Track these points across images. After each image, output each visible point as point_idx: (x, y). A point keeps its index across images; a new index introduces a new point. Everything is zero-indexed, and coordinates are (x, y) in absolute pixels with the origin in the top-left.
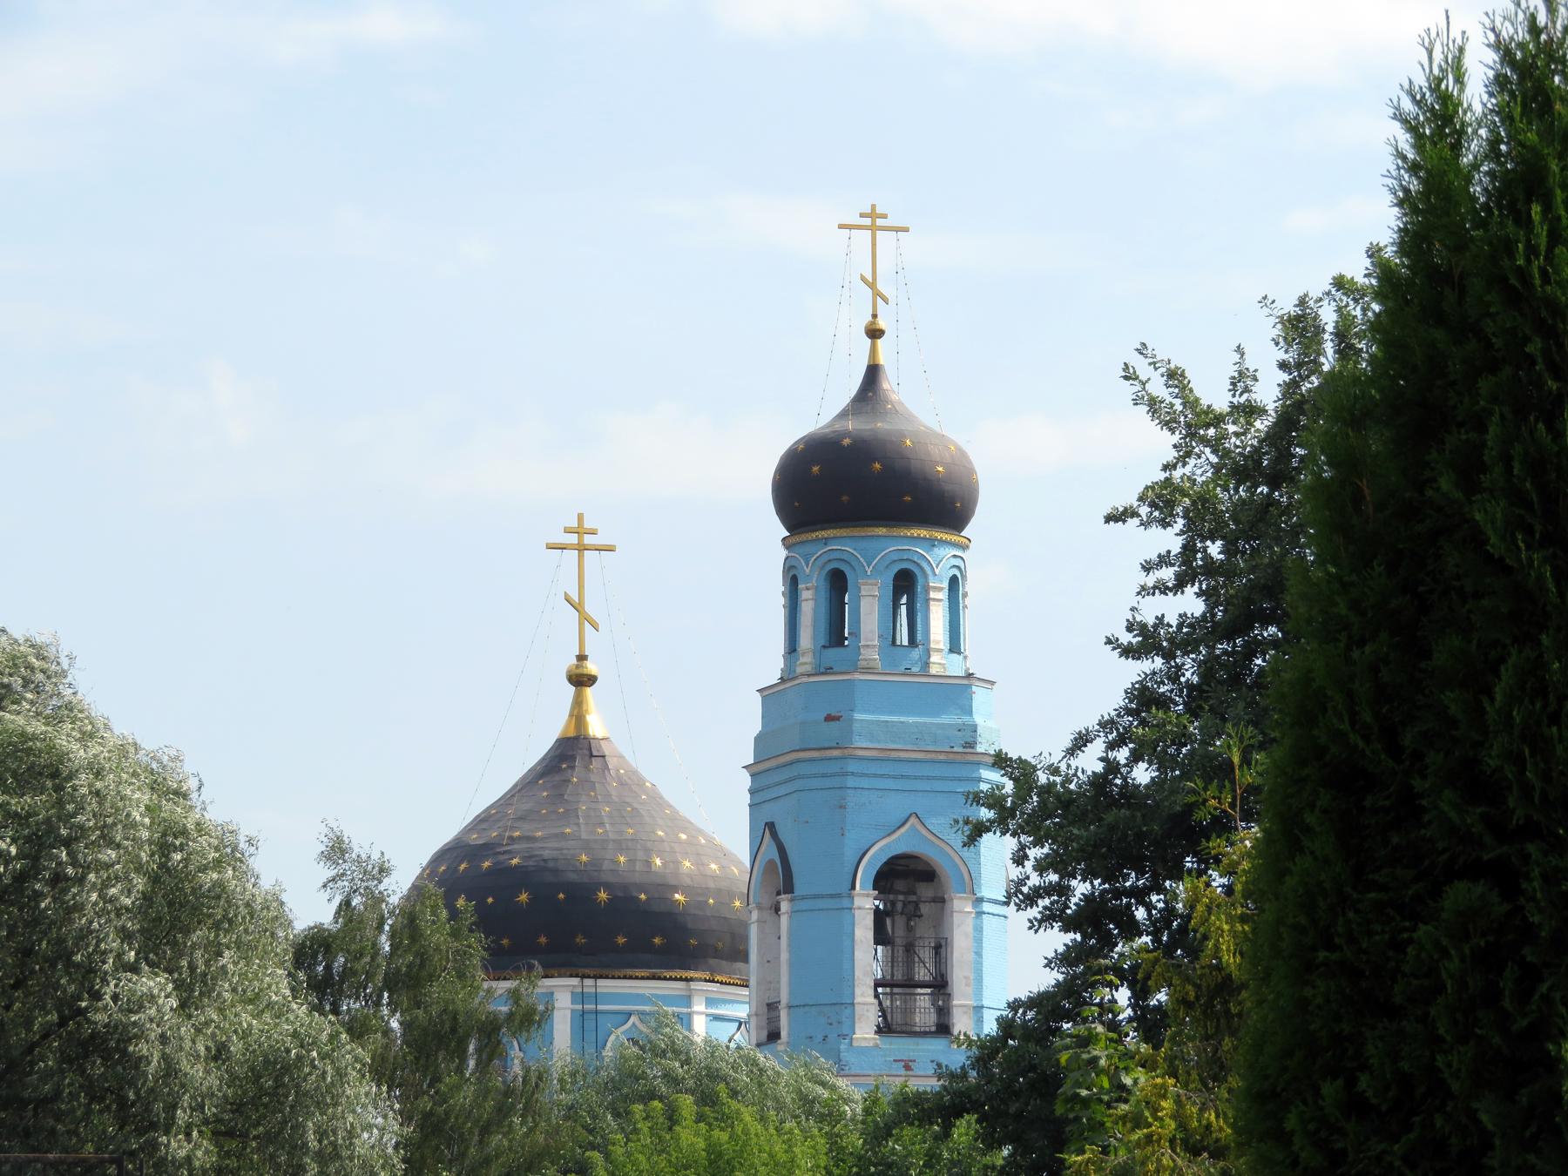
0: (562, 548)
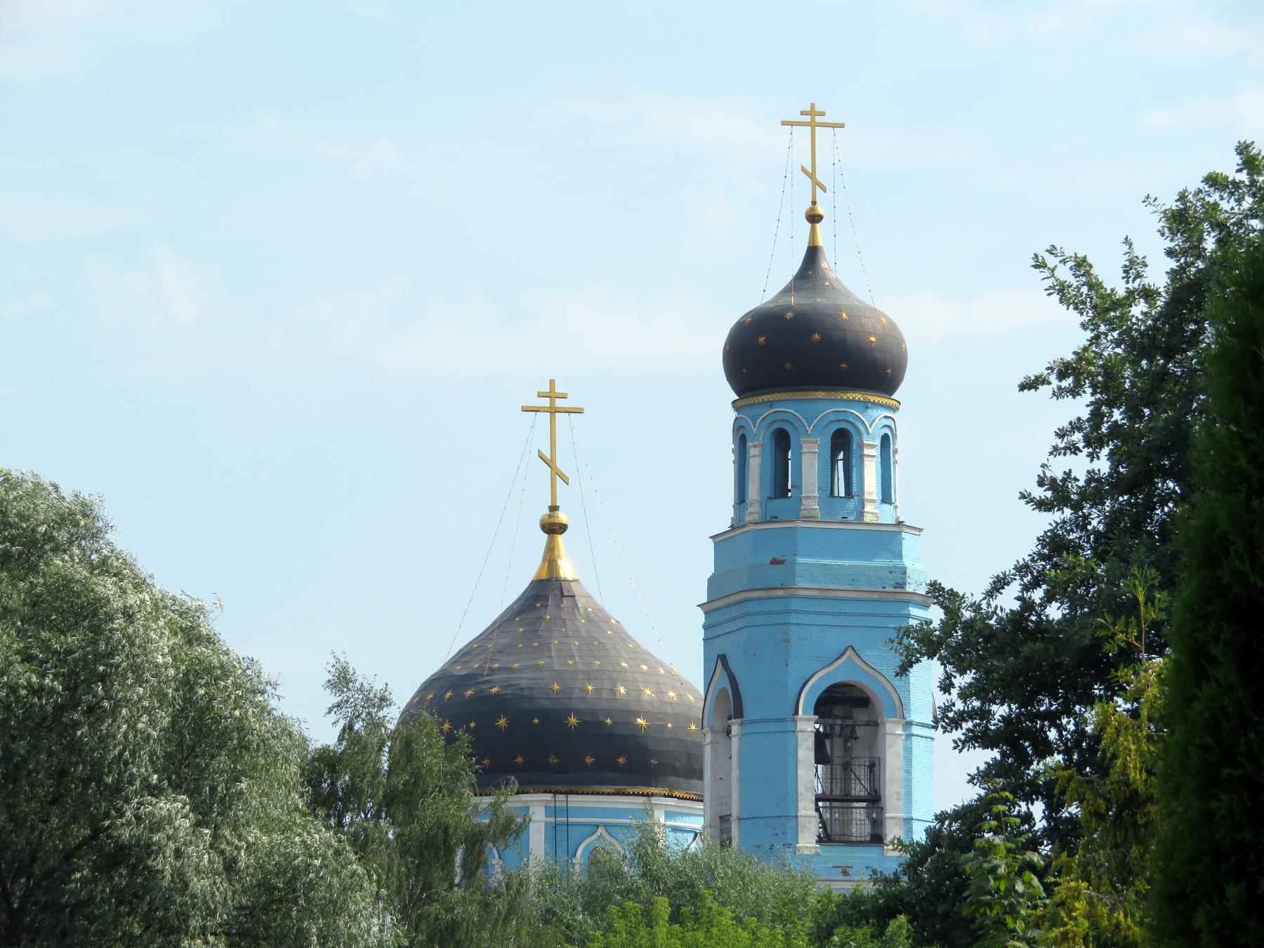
0: (792, 124)
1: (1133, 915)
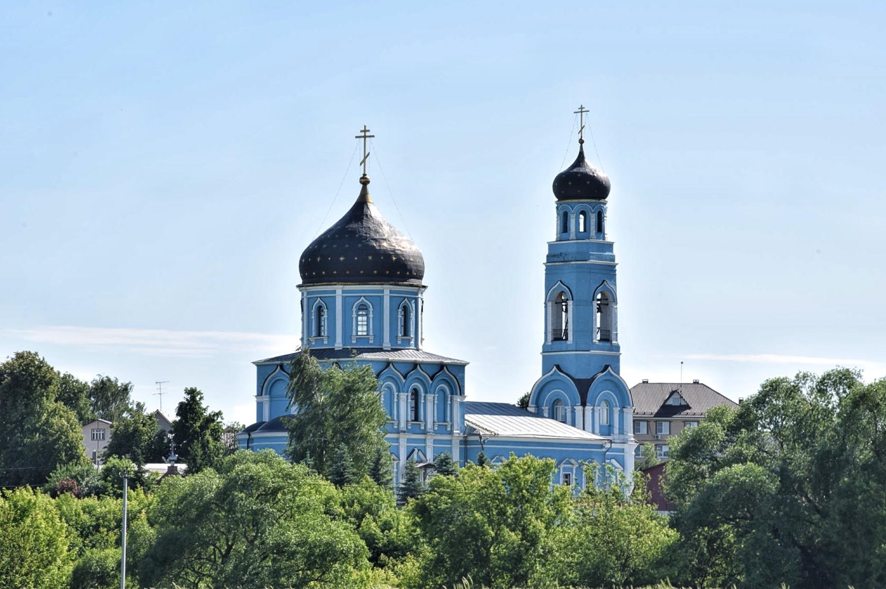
0: (577, 112)
1: (794, 435)
